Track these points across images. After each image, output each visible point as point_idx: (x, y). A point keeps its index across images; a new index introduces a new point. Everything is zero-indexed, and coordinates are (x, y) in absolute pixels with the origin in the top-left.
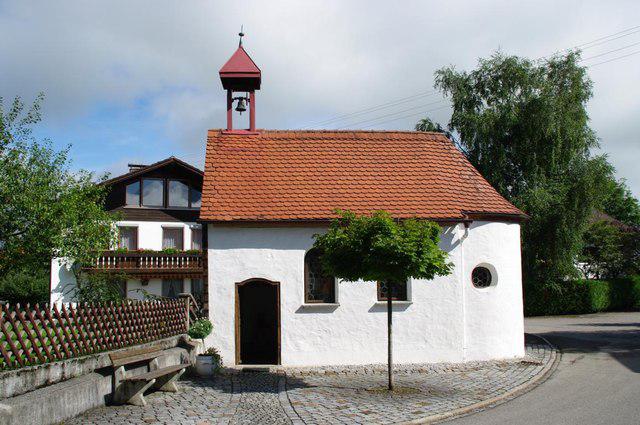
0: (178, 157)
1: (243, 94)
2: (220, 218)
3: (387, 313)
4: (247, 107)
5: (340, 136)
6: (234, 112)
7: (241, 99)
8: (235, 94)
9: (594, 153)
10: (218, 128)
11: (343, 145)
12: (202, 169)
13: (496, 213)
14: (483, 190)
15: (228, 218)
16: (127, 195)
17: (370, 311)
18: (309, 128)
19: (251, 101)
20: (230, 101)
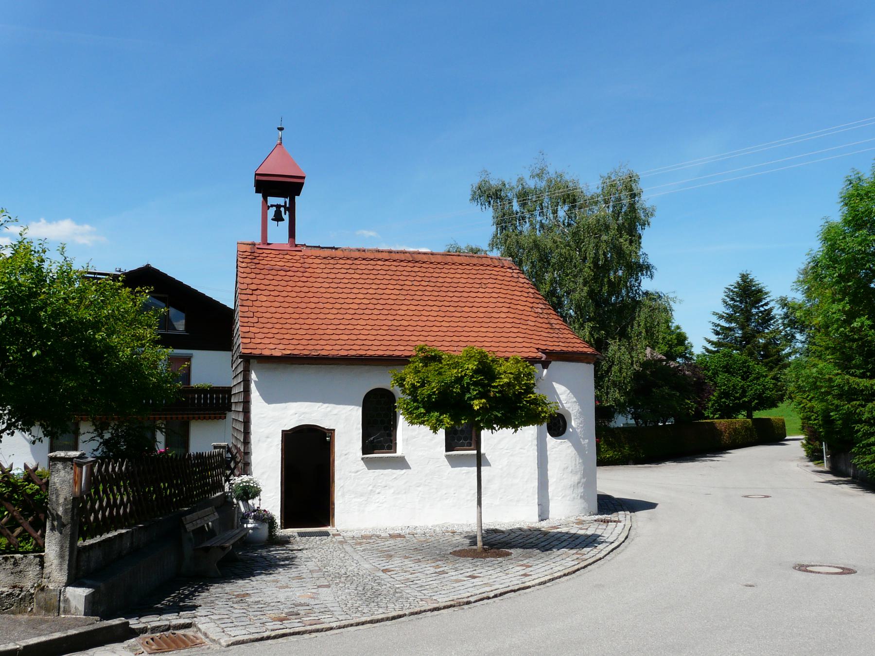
0: (154, 265)
1: (280, 201)
2: (267, 353)
3: (476, 468)
4: (286, 217)
5: (396, 257)
6: (271, 224)
7: (278, 207)
8: (272, 200)
9: (647, 284)
10: (250, 241)
11: (400, 268)
12: (224, 295)
13: (573, 353)
14: (557, 326)
15: (277, 353)
16: (175, 323)
17: (25, 464)
18: (360, 247)
19: (291, 209)
20: (266, 207)
